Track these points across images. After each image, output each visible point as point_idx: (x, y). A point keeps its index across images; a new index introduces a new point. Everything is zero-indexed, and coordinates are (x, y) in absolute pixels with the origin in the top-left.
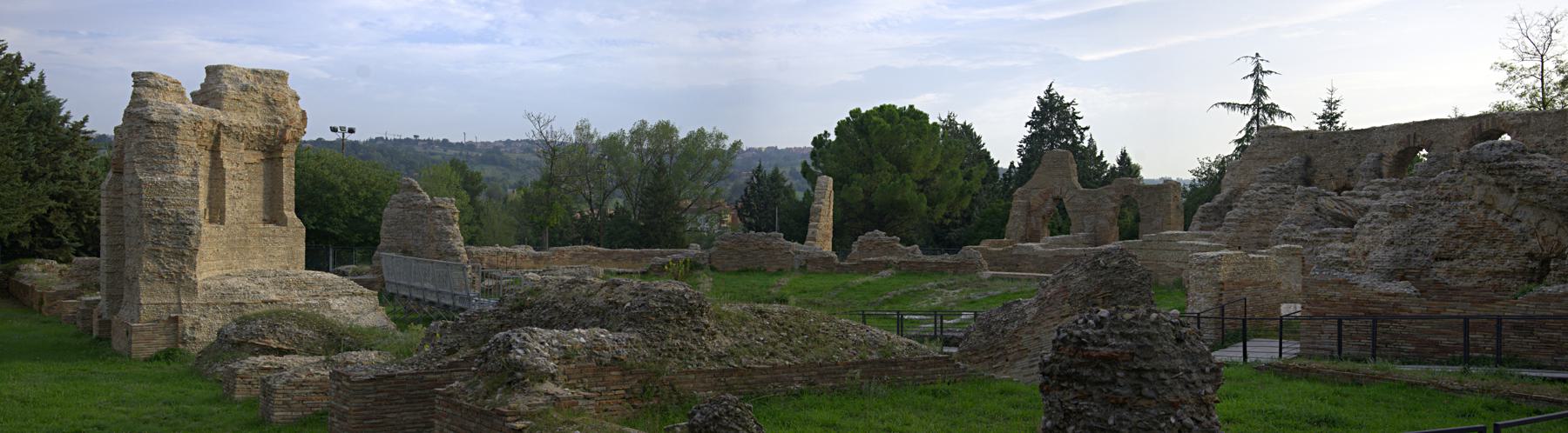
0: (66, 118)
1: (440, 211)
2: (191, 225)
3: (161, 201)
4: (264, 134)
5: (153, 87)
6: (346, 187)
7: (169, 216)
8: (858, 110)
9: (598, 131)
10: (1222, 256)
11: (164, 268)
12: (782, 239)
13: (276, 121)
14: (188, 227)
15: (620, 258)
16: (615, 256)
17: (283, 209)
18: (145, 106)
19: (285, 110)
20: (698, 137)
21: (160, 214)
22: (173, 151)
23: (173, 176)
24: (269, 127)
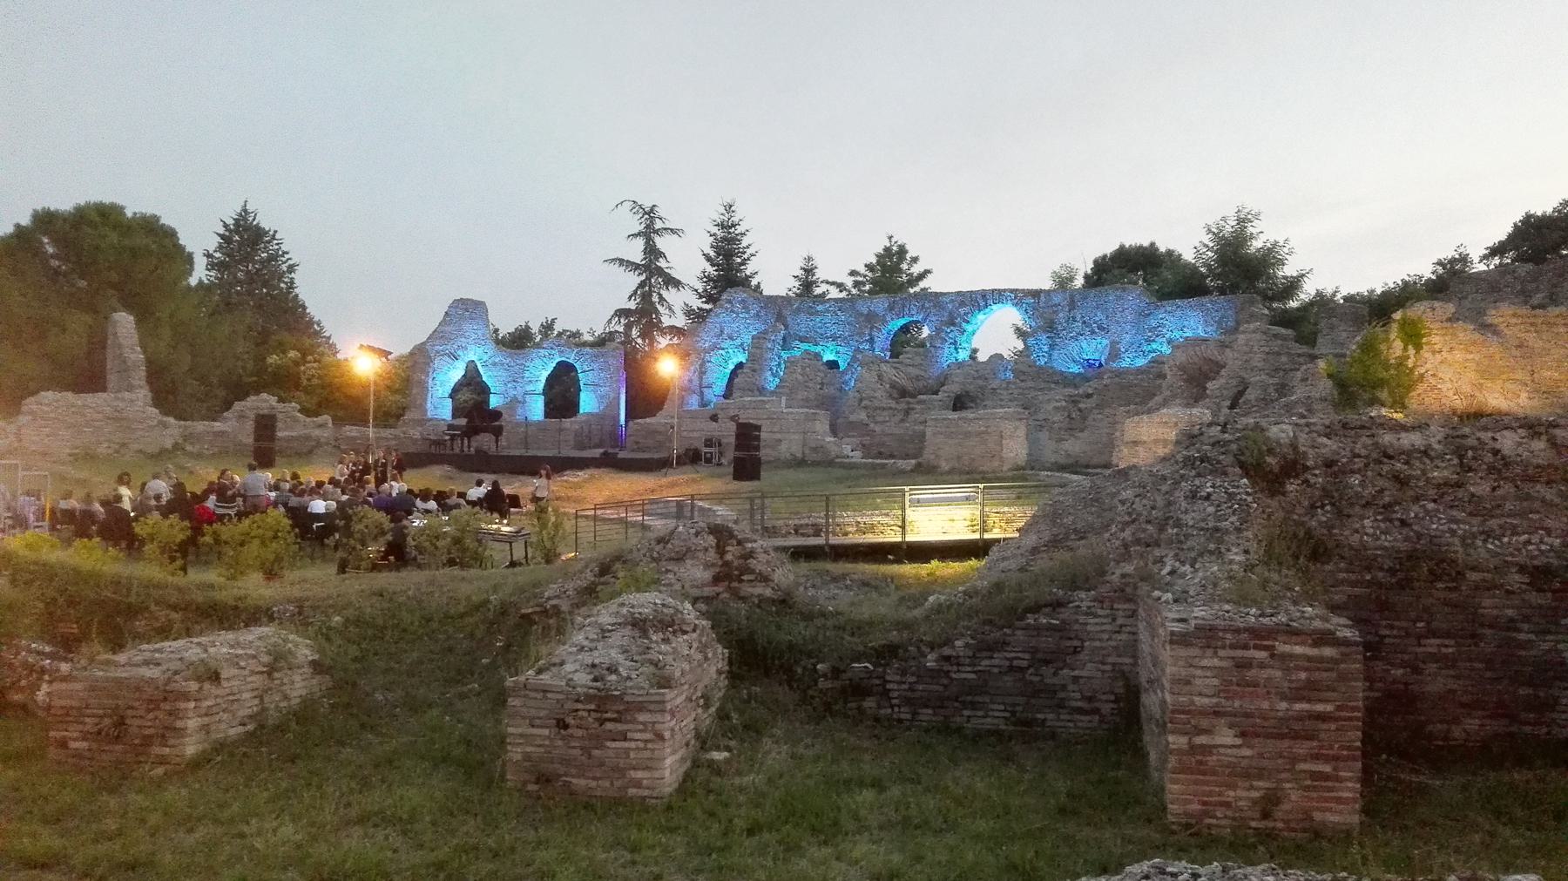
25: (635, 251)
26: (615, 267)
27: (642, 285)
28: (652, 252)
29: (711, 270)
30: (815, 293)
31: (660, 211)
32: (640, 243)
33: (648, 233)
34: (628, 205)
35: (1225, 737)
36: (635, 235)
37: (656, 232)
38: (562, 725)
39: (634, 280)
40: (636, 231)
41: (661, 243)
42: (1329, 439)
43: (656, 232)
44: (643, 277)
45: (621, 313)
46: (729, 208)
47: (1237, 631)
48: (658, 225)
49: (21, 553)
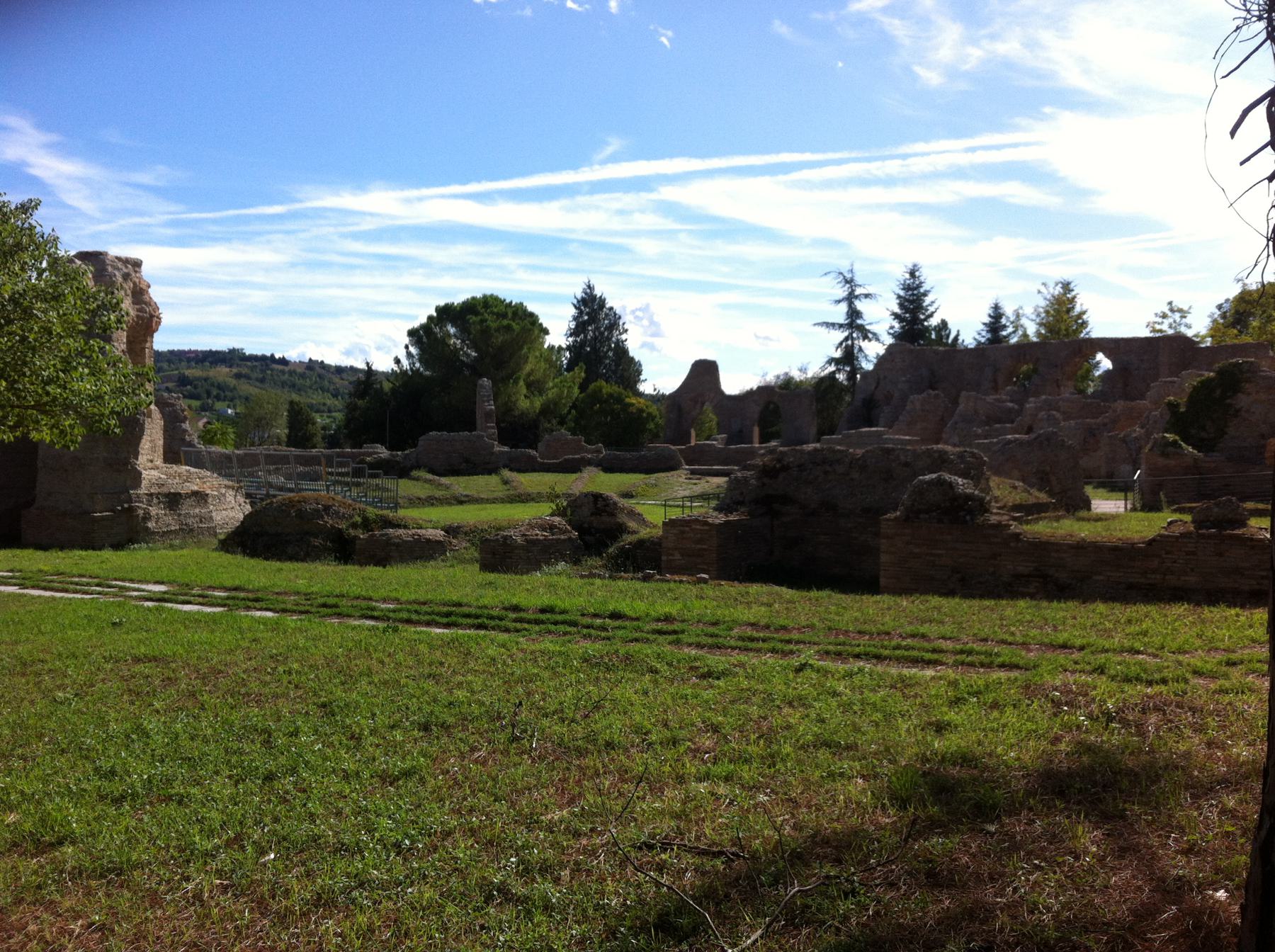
25: (840, 313)
26: (823, 330)
27: (846, 339)
28: (854, 314)
29: (897, 325)
30: (726, 479)
31: (858, 280)
32: (844, 307)
33: (851, 298)
34: (833, 275)
35: (677, 556)
36: (839, 301)
37: (857, 297)
38: (494, 554)
39: (840, 335)
40: (841, 297)
41: (860, 305)
42: (1180, 421)
43: (857, 297)
44: (846, 334)
45: (832, 361)
46: (912, 274)
47: (298, 593)
48: (858, 291)
49: (931, 598)
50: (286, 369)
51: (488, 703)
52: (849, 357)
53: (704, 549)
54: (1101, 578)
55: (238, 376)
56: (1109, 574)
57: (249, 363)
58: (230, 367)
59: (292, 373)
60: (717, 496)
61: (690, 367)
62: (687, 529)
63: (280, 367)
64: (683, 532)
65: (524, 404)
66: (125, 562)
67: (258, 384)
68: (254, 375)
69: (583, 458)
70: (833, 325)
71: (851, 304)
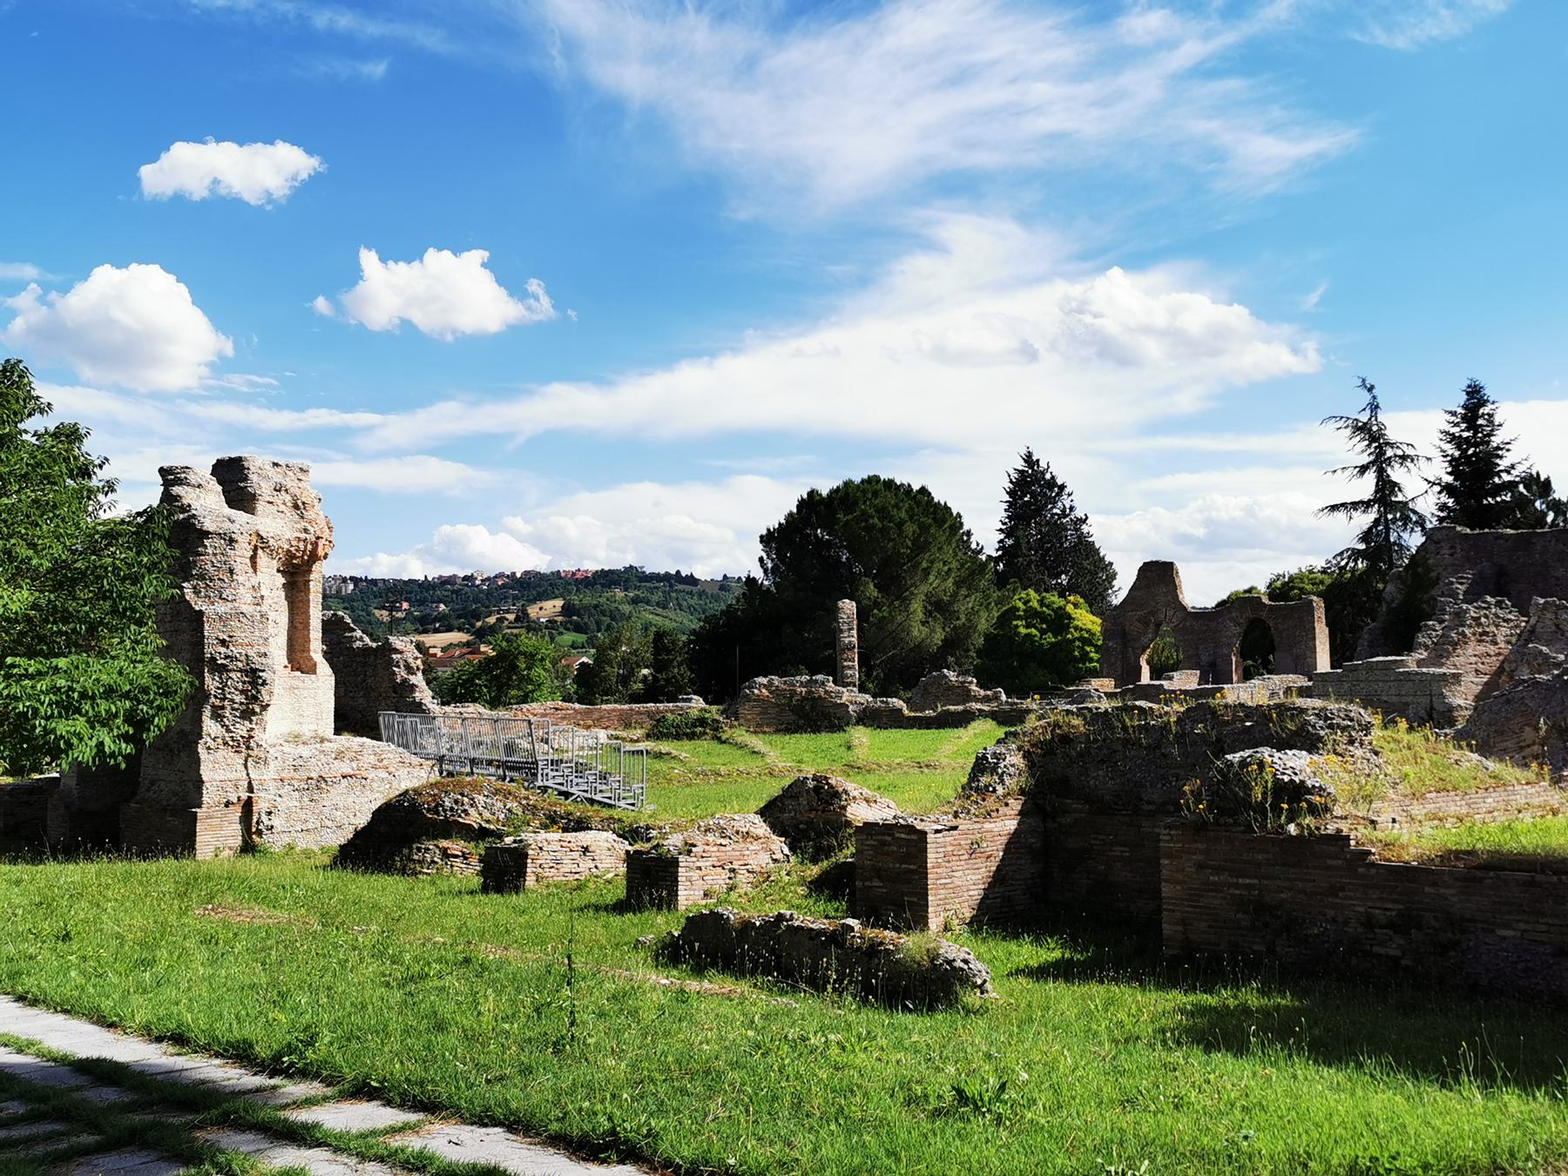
0: (1443, 507)
1: (399, 656)
2: (263, 671)
3: (228, 639)
4: (292, 549)
5: (194, 486)
6: (916, 592)
7: (237, 660)
8: (762, 537)
9: (981, 543)
10: (718, 755)
11: (228, 731)
12: (831, 684)
13: (306, 530)
14: (261, 674)
15: (602, 718)
16: (597, 715)
17: (309, 651)
18: (189, 511)
19: (314, 516)
20: (526, 573)
21: (226, 657)
22: (231, 571)
23: (236, 605)
24: (299, 539)
26: (1341, 516)
28: (1385, 488)
32: (1371, 478)
33: (1380, 463)
41: (1396, 473)
50: (695, 589)
51: (1226, 1144)
52: (1376, 545)
53: (912, 871)
54: (1508, 933)
55: (635, 601)
56: (1522, 926)
57: (648, 584)
58: (626, 590)
59: (701, 594)
60: (1317, 753)
61: (1136, 573)
62: (889, 838)
63: (688, 588)
64: (883, 843)
65: (917, 631)
66: (711, 823)
67: (660, 611)
68: (655, 598)
69: (966, 711)
70: (1355, 505)
71: (1381, 473)
